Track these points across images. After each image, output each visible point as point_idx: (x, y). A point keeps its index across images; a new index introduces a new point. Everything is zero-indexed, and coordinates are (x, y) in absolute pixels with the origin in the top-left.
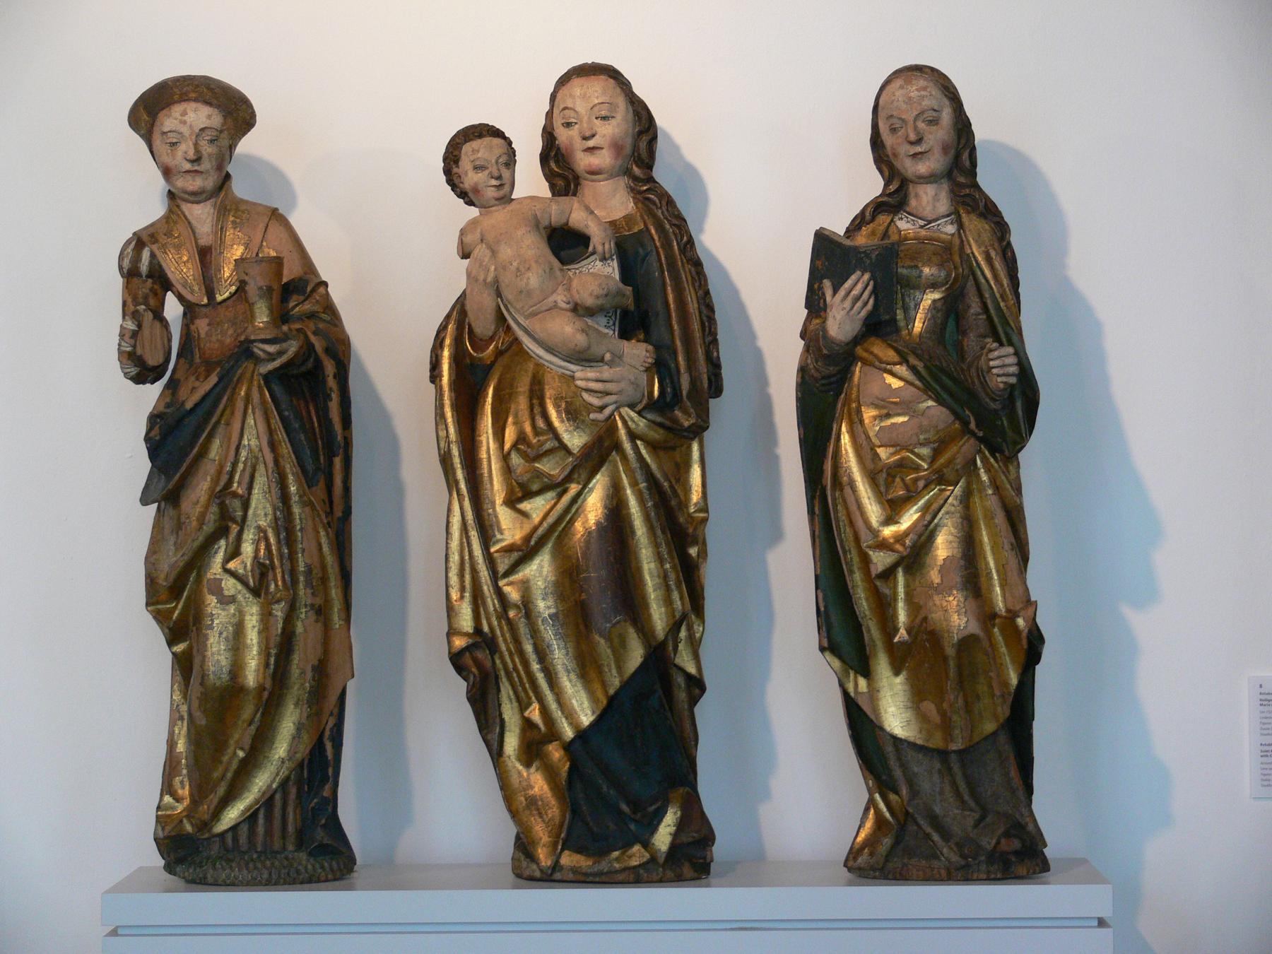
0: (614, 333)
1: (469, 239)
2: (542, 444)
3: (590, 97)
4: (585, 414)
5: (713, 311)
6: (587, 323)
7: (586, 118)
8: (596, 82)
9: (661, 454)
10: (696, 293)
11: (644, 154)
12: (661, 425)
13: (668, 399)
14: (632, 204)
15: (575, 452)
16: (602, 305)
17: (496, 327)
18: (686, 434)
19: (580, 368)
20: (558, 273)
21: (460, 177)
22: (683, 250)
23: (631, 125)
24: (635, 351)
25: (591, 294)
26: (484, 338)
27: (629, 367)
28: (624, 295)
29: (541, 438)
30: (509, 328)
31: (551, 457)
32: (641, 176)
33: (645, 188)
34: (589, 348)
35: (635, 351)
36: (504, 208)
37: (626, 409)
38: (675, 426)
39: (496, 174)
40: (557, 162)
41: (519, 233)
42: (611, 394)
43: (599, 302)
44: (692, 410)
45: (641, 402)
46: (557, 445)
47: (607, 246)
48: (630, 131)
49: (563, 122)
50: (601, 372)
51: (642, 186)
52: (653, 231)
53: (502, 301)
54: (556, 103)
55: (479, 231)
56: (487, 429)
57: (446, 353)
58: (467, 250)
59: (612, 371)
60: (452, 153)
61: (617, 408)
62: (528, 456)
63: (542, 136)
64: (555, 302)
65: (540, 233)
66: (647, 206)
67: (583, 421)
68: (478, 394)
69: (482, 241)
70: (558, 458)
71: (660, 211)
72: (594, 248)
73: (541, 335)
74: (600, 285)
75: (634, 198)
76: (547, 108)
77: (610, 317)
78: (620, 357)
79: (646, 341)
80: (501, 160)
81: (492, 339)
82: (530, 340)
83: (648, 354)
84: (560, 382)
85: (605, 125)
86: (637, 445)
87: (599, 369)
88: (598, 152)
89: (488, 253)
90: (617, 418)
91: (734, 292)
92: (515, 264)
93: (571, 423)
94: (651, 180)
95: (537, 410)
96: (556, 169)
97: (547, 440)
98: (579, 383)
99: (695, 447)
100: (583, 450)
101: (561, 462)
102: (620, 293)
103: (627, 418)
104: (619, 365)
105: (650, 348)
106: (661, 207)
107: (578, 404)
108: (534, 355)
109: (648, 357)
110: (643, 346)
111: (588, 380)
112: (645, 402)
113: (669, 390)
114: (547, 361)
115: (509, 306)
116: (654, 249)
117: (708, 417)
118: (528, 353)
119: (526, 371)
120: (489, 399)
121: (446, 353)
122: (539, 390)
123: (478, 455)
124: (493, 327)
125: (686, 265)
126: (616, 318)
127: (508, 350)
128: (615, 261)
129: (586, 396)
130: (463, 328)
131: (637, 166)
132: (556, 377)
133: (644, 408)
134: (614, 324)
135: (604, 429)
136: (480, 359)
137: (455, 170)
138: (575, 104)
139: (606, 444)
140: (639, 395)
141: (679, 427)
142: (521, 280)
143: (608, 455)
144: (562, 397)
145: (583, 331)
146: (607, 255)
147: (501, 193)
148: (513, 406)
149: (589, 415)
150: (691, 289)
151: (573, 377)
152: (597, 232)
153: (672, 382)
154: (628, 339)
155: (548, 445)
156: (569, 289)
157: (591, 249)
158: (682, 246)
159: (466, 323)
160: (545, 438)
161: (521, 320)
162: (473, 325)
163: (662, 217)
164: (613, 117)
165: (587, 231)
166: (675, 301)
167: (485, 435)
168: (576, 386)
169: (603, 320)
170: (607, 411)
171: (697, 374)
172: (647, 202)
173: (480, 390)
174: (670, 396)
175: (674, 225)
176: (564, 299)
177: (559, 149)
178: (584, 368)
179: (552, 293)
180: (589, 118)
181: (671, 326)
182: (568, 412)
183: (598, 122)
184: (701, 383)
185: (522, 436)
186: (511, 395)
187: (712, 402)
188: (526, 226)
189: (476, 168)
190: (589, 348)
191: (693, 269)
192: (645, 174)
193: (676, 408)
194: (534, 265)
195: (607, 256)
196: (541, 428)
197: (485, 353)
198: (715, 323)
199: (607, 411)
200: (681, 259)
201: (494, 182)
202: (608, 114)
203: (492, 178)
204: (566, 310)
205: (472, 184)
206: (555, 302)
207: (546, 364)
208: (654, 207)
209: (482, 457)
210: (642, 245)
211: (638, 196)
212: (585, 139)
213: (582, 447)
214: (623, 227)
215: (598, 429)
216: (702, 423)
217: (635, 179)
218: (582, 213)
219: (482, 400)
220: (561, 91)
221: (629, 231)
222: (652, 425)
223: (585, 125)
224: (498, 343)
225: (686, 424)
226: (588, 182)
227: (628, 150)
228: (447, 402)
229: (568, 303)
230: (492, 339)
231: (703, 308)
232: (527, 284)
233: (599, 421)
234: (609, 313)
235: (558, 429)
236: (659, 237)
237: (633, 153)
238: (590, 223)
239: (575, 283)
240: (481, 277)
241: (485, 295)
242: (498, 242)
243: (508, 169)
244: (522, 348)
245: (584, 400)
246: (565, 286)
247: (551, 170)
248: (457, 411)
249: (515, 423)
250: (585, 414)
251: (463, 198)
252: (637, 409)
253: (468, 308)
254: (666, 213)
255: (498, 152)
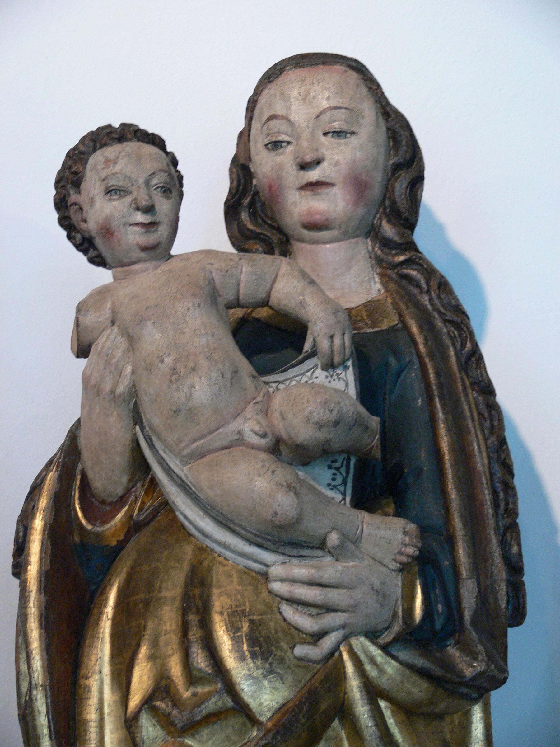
0: (344, 499)
1: (89, 319)
2: (203, 700)
3: (314, 98)
4: (286, 646)
5: (512, 475)
6: (297, 475)
7: (306, 135)
8: (327, 75)
9: (421, 725)
10: (486, 440)
11: (402, 204)
12: (423, 673)
13: (438, 625)
14: (378, 286)
15: (263, 719)
16: (327, 442)
17: (130, 481)
18: (464, 690)
19: (280, 558)
20: (248, 382)
21: (81, 209)
22: (464, 367)
23: (382, 150)
24: (382, 533)
25: (308, 420)
26: (109, 500)
27: (371, 562)
28: (367, 428)
29: (200, 690)
30: (154, 484)
31: (216, 727)
32: (397, 238)
33: (402, 258)
34: (299, 520)
35: (382, 533)
36: (156, 268)
37: (362, 639)
38: (449, 675)
39: (144, 203)
40: (253, 215)
41: (181, 307)
42: (335, 610)
43: (322, 435)
44: (480, 647)
45: (388, 628)
46: (229, 703)
47: (337, 341)
48: (381, 160)
49: (266, 141)
50: (319, 568)
51: (398, 254)
52: (415, 329)
53: (142, 428)
54: (257, 112)
55: (109, 305)
56: (102, 666)
57: (38, 523)
58: (86, 340)
59: (340, 566)
60: (70, 168)
61: (346, 638)
62: (172, 724)
63: (231, 171)
64: (239, 432)
65: (218, 311)
66: (403, 288)
67: (282, 660)
68: (91, 601)
69: (113, 323)
70: (229, 731)
71: (426, 298)
72: (314, 345)
73: (210, 493)
74: (325, 403)
75: (382, 276)
76: (241, 125)
77: (337, 469)
78: (356, 542)
79: (397, 514)
80: (154, 181)
81: (122, 500)
82: (189, 502)
83: (407, 539)
84: (241, 582)
85: (340, 145)
86: (379, 708)
87: (313, 562)
88: (325, 190)
89: (122, 343)
90: (345, 656)
91: (527, 457)
92: (168, 360)
93: (259, 662)
94: (411, 246)
95: (195, 634)
96: (251, 227)
97: (209, 695)
98: (276, 586)
99: (477, 714)
100: (278, 716)
101: (234, 738)
102: (359, 423)
103: (362, 657)
104: (354, 557)
105: (411, 527)
106: (428, 291)
107: (272, 624)
108: (193, 531)
109: (406, 545)
110: (400, 522)
111: (293, 581)
112: (397, 628)
113: (440, 607)
114: (219, 543)
115: (154, 439)
116: (415, 359)
117: (505, 661)
118: (183, 527)
119: (179, 560)
120: (109, 610)
121: (38, 523)
122: (201, 596)
123: (80, 714)
124: (125, 480)
125: (470, 391)
126: (347, 472)
127: (151, 520)
128: (350, 372)
129: (288, 611)
130: (72, 477)
131: (389, 221)
132: (233, 572)
133: (396, 640)
134: (344, 482)
135: (320, 676)
136: (99, 536)
137: (73, 197)
138: (289, 108)
139: (323, 706)
140: (387, 615)
141: (456, 679)
142: (178, 389)
143: (326, 726)
144: (243, 612)
145: (289, 486)
146: (337, 359)
147: (151, 239)
148: (150, 625)
149: (292, 648)
150: (479, 432)
151: (265, 576)
152: (321, 315)
153: (444, 589)
154: (371, 510)
155: (212, 705)
156: (266, 412)
157: (307, 346)
158: (463, 360)
159: (78, 471)
160: (207, 689)
161: (175, 465)
162: (90, 474)
163: (429, 307)
164: (353, 133)
165: (303, 314)
166: (452, 450)
167: (96, 677)
168: (270, 592)
169: (326, 475)
170: (328, 643)
171: (488, 582)
172: (404, 282)
173: (96, 591)
174: (442, 618)
175: (450, 322)
176: (257, 428)
177: (257, 193)
178: (287, 559)
179: (235, 417)
180: (313, 133)
181: (444, 492)
182: (253, 641)
183: (327, 141)
184: (496, 598)
185: (163, 683)
186: (147, 603)
187: (511, 632)
188: (193, 295)
189: (109, 191)
190: (299, 520)
191: (481, 399)
192: (402, 236)
193: (451, 642)
194: (203, 363)
195: (337, 359)
196: (200, 670)
197: (108, 526)
198: (515, 495)
199: (328, 643)
200: (462, 379)
201: (140, 217)
202: (345, 127)
203: (138, 209)
204: (258, 448)
205: (101, 221)
206: (239, 432)
207: (218, 548)
208: (415, 291)
209: (88, 717)
210: (396, 353)
211: (389, 272)
212: (304, 166)
213: (278, 710)
214: (362, 320)
215: (309, 676)
216: (496, 673)
217: (386, 243)
218: (296, 283)
219: (95, 611)
220: (266, 91)
221: (373, 326)
222: (404, 669)
223: (305, 144)
224: (131, 509)
225: (469, 672)
226: (303, 245)
227: (376, 191)
228: (33, 611)
229: (264, 436)
230: (122, 500)
231: (496, 468)
232: (189, 397)
233: (311, 661)
234: (335, 461)
235: (234, 673)
236: (426, 340)
237: (383, 201)
238: (308, 299)
239: (278, 401)
240: (107, 386)
241: (112, 420)
242: (141, 320)
243: (168, 198)
244: (175, 517)
245: (285, 620)
246: (259, 406)
247: (242, 229)
248: (47, 632)
249: (152, 657)
250: (286, 646)
251: (85, 252)
252: (381, 641)
253: (83, 443)
254: (436, 301)
255: (150, 166)
